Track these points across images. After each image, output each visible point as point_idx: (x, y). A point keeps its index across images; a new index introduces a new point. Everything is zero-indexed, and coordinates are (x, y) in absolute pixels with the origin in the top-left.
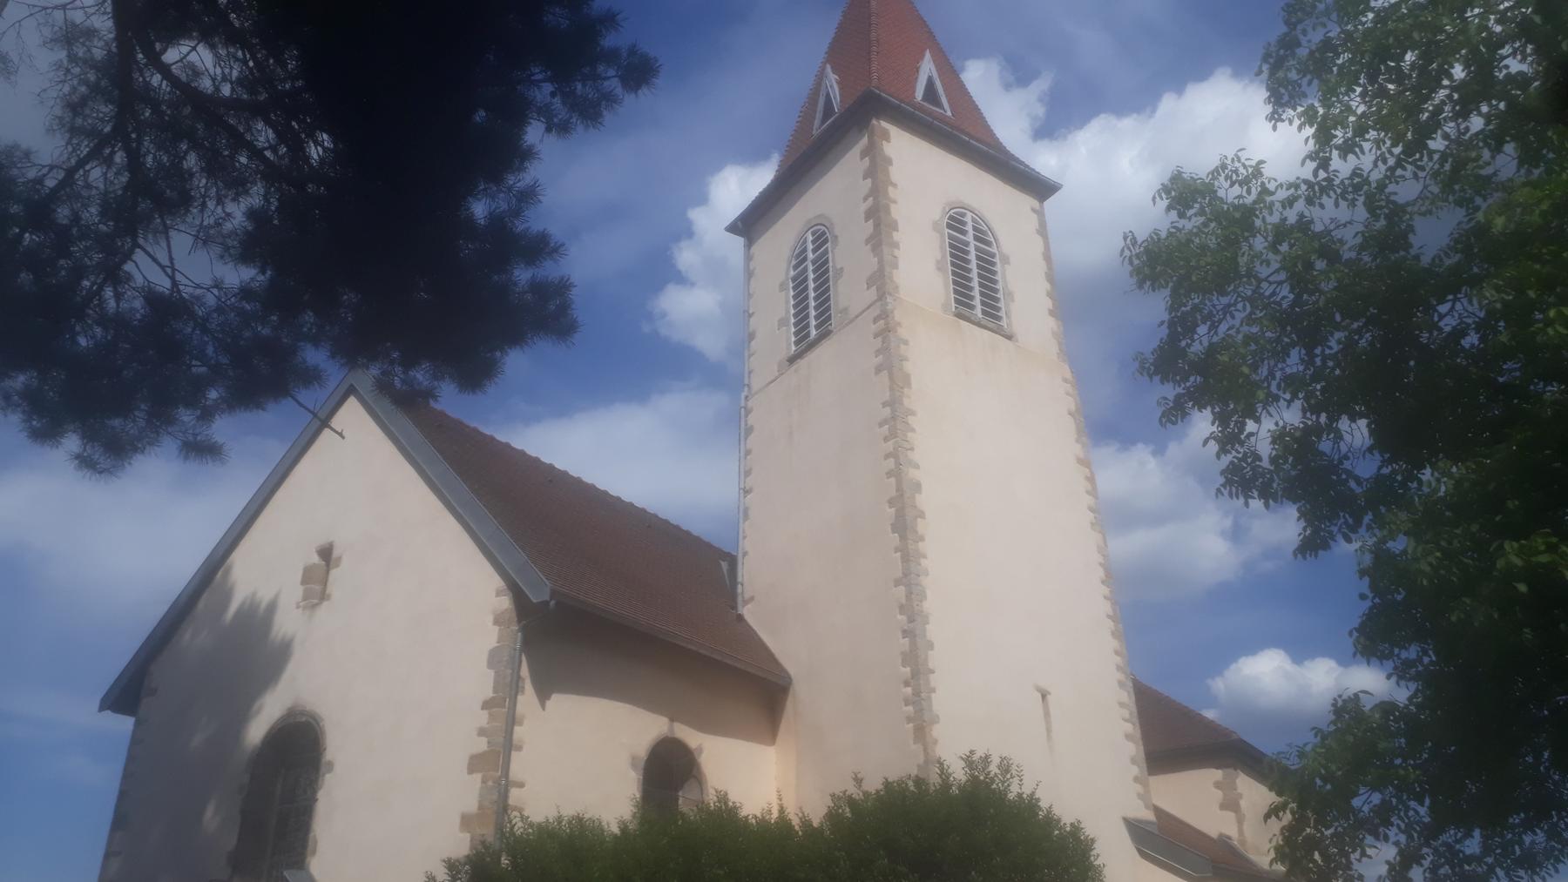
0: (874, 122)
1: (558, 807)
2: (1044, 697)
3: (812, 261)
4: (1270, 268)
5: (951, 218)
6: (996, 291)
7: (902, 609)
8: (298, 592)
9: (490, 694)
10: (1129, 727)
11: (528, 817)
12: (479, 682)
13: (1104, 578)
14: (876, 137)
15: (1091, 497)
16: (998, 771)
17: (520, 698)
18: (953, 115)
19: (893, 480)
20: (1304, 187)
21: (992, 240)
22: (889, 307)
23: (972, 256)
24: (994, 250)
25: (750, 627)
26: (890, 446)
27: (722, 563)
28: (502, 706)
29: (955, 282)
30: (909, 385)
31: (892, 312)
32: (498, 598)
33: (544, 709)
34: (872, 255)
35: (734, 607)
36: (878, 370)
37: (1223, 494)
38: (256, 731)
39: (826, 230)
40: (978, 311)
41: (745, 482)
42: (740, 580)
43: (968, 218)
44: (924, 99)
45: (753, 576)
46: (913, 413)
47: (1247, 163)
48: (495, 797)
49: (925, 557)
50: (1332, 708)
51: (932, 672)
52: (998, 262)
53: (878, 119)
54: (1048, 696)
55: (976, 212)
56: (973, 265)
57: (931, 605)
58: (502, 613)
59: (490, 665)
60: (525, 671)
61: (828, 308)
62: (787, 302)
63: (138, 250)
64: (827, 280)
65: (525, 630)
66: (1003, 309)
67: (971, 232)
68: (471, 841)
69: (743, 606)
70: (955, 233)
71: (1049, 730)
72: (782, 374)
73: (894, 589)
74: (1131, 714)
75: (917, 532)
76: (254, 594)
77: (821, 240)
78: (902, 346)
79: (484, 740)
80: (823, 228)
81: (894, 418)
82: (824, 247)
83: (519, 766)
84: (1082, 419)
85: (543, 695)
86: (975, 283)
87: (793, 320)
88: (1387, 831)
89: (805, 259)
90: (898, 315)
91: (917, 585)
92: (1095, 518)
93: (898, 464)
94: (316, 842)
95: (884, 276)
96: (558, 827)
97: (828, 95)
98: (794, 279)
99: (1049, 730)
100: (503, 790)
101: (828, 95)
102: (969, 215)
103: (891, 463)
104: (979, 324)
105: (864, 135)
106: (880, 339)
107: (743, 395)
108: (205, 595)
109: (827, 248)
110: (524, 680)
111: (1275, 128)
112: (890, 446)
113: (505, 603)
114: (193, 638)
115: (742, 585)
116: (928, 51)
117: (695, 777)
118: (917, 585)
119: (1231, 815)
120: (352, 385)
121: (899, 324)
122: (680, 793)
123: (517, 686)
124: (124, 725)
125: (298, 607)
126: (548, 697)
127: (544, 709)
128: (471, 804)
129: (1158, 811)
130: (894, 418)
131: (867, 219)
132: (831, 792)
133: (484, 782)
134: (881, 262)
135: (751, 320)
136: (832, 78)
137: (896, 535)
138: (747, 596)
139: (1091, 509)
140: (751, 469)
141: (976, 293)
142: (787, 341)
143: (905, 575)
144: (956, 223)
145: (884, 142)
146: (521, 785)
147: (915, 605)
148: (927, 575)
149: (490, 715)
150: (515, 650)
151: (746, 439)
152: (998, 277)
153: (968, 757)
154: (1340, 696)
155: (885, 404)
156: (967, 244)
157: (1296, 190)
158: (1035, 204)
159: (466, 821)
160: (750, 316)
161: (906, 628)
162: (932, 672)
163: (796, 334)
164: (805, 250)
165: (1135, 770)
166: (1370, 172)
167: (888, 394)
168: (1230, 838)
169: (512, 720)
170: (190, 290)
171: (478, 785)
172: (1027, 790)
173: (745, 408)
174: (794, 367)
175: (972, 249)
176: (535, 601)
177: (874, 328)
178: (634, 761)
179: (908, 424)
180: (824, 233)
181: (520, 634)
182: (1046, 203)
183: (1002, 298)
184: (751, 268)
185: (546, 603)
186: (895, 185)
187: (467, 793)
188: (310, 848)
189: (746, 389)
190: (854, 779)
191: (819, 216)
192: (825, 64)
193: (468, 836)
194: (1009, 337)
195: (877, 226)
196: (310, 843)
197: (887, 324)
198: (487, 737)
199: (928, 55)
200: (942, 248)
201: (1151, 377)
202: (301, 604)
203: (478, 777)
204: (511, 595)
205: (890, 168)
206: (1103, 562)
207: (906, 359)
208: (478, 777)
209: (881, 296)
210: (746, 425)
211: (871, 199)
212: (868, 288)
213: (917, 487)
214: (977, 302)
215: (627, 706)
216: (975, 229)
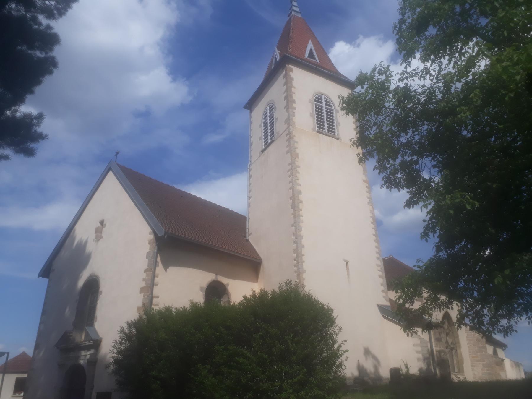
1: (338, 316)
2: (347, 263)
4: (390, 103)
9: (146, 267)
12: (143, 263)
13: (372, 221)
15: (368, 194)
18: (320, 62)
19: (291, 190)
23: (324, 111)
24: (333, 108)
26: (290, 179)
28: (151, 271)
29: (317, 120)
31: (292, 132)
33: (166, 272)
34: (286, 112)
35: (246, 237)
36: (287, 152)
38: (81, 283)
40: (326, 131)
42: (247, 227)
43: (323, 98)
44: (308, 57)
45: (251, 226)
46: (299, 167)
48: (148, 301)
49: (302, 216)
52: (334, 113)
53: (288, 64)
54: (348, 263)
55: (326, 95)
60: (159, 259)
67: (324, 103)
71: (348, 275)
74: (381, 269)
77: (271, 108)
78: (296, 144)
81: (292, 169)
83: (156, 291)
85: (166, 267)
87: (263, 137)
88: (452, 306)
89: (267, 116)
90: (294, 133)
92: (370, 201)
93: (293, 185)
95: (290, 119)
98: (264, 123)
99: (348, 275)
101: (276, 58)
102: (323, 96)
104: (326, 135)
106: (288, 142)
107: (249, 165)
112: (290, 179)
113: (152, 237)
114: (64, 254)
115: (248, 229)
117: (227, 294)
120: (110, 167)
122: (222, 299)
124: (45, 281)
125: (94, 241)
127: (166, 272)
130: (292, 169)
137: (292, 209)
139: (368, 198)
140: (251, 190)
143: (295, 223)
144: (318, 99)
145: (291, 72)
146: (158, 297)
149: (146, 274)
150: (155, 252)
152: (334, 118)
153: (286, 282)
155: (289, 164)
164: (267, 113)
165: (382, 288)
169: (154, 276)
173: (249, 169)
174: (264, 153)
176: (159, 236)
177: (286, 138)
178: (201, 289)
179: (297, 171)
181: (156, 247)
186: (294, 87)
188: (95, 320)
189: (250, 163)
194: (338, 139)
195: (288, 102)
197: (290, 136)
198: (145, 281)
199: (310, 41)
200: (312, 109)
202: (95, 240)
203: (142, 295)
205: (293, 81)
206: (372, 216)
207: (297, 148)
208: (142, 295)
211: (286, 93)
212: (285, 124)
213: (300, 192)
215: (199, 270)
216: (325, 101)
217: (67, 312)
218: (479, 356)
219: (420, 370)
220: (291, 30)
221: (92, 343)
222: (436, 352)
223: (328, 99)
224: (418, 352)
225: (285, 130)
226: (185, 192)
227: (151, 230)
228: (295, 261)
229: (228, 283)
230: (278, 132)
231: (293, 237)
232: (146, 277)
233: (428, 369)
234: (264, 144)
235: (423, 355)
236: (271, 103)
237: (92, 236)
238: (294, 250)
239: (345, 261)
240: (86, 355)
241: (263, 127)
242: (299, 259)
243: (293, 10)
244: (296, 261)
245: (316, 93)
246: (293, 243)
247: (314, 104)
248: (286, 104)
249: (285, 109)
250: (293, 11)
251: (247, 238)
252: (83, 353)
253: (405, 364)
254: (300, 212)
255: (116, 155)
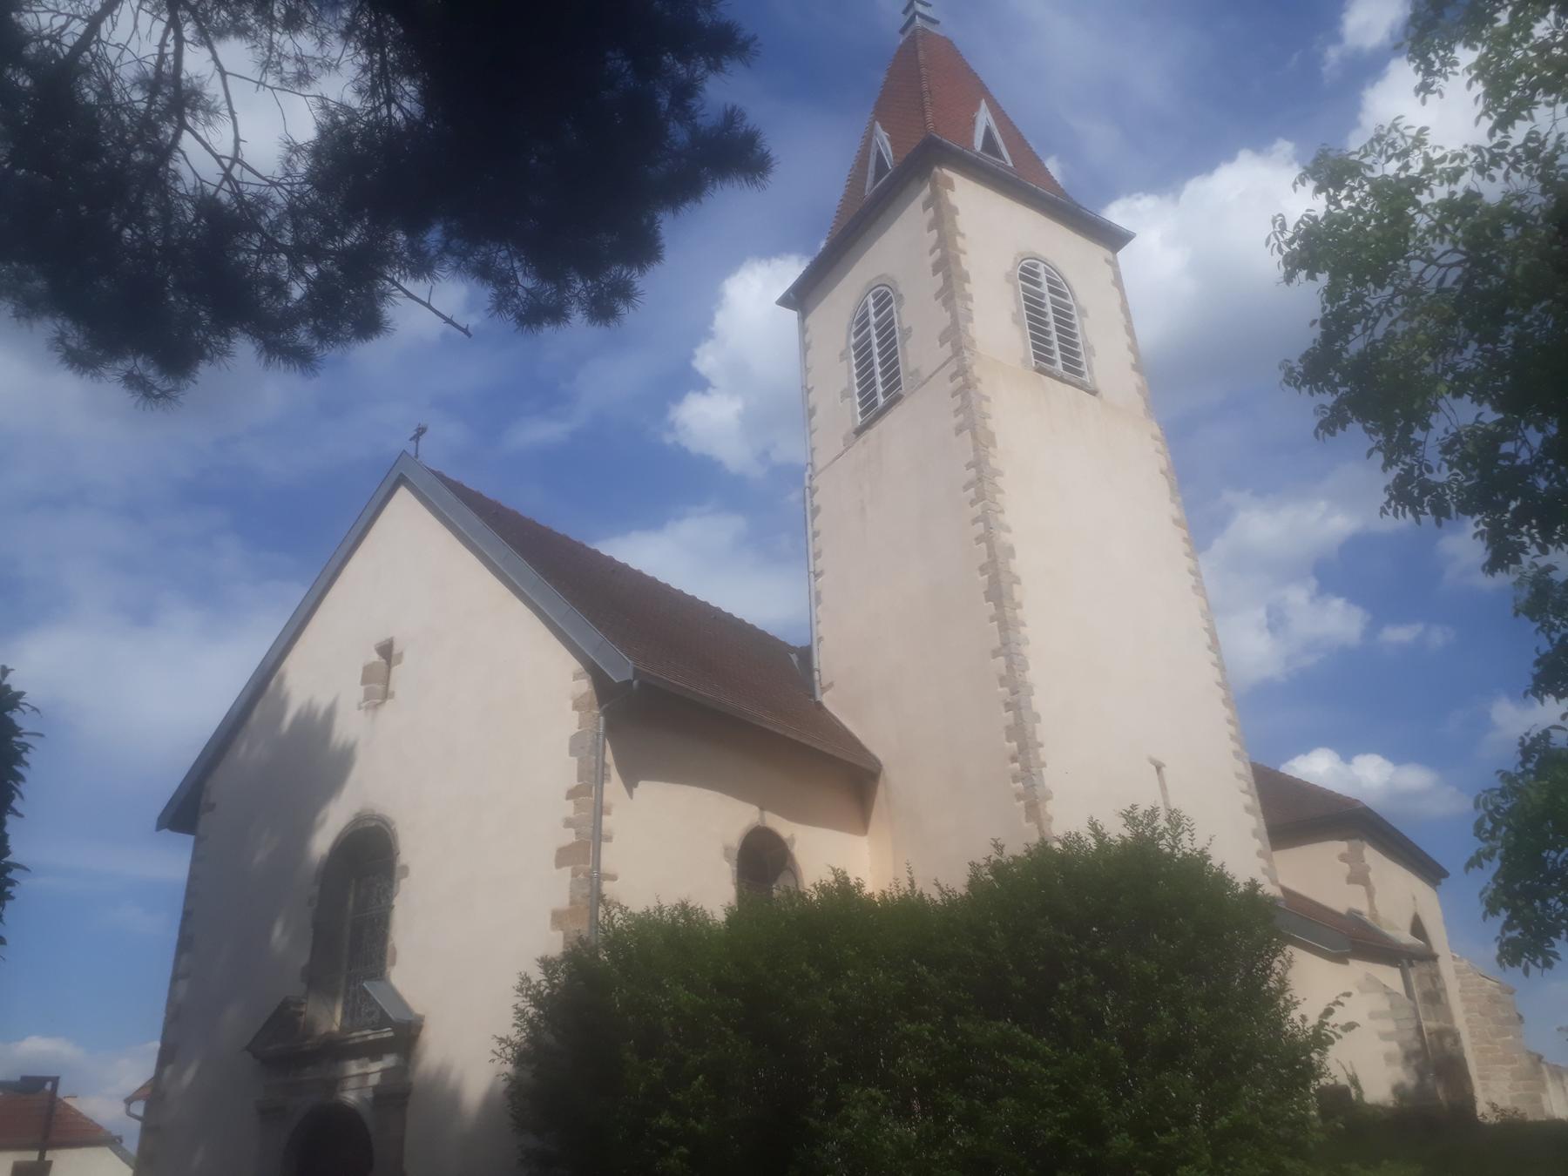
0: (936, 170)
2: (1159, 768)
3: (853, 347)
5: (1023, 269)
6: (1076, 345)
7: (1002, 681)
8: (359, 692)
9: (573, 782)
10: (1248, 799)
11: (627, 908)
12: (564, 771)
14: (938, 186)
16: (1167, 826)
17: (606, 785)
19: (983, 545)
20: (1472, 156)
21: (1068, 291)
22: (968, 362)
23: (1049, 309)
24: (1070, 301)
25: (829, 713)
27: (791, 656)
28: (588, 793)
30: (993, 443)
31: (971, 367)
32: (577, 682)
33: (631, 798)
34: (943, 309)
35: (813, 695)
36: (959, 430)
37: (1387, 513)
38: (322, 843)
39: (889, 291)
41: (814, 565)
42: (816, 666)
43: (1041, 269)
45: (827, 664)
47: (1408, 132)
48: (587, 891)
49: (1024, 625)
50: (1520, 748)
51: (1041, 745)
55: (1049, 263)
56: (1050, 318)
57: (1034, 674)
58: (581, 697)
59: (572, 752)
60: (609, 757)
61: (897, 372)
62: (850, 371)
63: (185, 132)
64: (894, 343)
65: (608, 713)
66: (1085, 363)
67: (1045, 284)
68: (565, 938)
69: (822, 694)
70: (1028, 285)
72: (849, 447)
73: (993, 660)
74: (1249, 785)
75: (1013, 599)
76: (310, 702)
79: (572, 831)
80: (885, 289)
81: (980, 480)
82: (866, 330)
83: (610, 857)
84: (1175, 478)
85: (630, 782)
86: (1054, 336)
87: (857, 390)
89: (867, 324)
90: (976, 370)
91: (1018, 654)
93: (988, 528)
94: (395, 953)
95: (959, 329)
96: (659, 918)
97: (879, 154)
98: (855, 347)
100: (595, 883)
103: (980, 528)
104: (1061, 379)
105: (926, 186)
106: (958, 397)
107: (807, 474)
108: (259, 705)
109: (892, 309)
110: (609, 766)
111: (1424, 102)
113: (585, 686)
114: (246, 751)
115: (819, 671)
116: (983, 100)
118: (1018, 654)
119: (1361, 889)
120: (401, 475)
121: (979, 380)
123: (603, 774)
125: (360, 708)
126: (636, 785)
127: (631, 798)
128: (562, 900)
129: (1284, 890)
130: (980, 480)
131: (935, 272)
132: (970, 861)
133: (574, 875)
134: (954, 317)
135: (810, 396)
136: (882, 137)
137: (992, 603)
138: (825, 683)
139: (1192, 572)
141: (1056, 346)
142: (852, 411)
143: (1004, 645)
144: (1028, 274)
145: (948, 190)
146: (613, 878)
147: (1017, 676)
148: (1028, 643)
151: (812, 521)
152: (1077, 330)
153: (1129, 812)
154: (1527, 734)
155: (969, 466)
156: (1042, 296)
157: (1462, 162)
158: (1107, 253)
159: (558, 918)
160: (809, 391)
161: (1008, 700)
162: (1041, 745)
163: (861, 404)
164: (866, 314)
165: (1257, 844)
166: (1548, 134)
167: (972, 454)
168: (1360, 913)
169: (600, 810)
170: (254, 189)
171: (568, 878)
172: (1198, 845)
173: (809, 488)
175: (1047, 301)
176: (617, 681)
177: (951, 386)
180: (887, 294)
181: (602, 718)
182: (1119, 254)
183: (1083, 353)
184: (807, 341)
185: (629, 683)
186: (963, 236)
187: (558, 888)
190: (994, 846)
191: (880, 277)
192: (874, 121)
193: (560, 934)
194: (1094, 393)
196: (389, 954)
197: (966, 380)
198: (574, 828)
201: (1299, 388)
202: (363, 705)
203: (567, 870)
204: (590, 678)
205: (957, 217)
208: (567, 870)
209: (958, 351)
210: (812, 505)
213: (1011, 552)
214: (1057, 356)
216: (1049, 280)
217: (278, 934)
218: (1499, 1047)
219: (1398, 1090)
220: (923, 70)
221: (391, 1034)
222: (1430, 1034)
223: (1057, 275)
224: (1385, 1036)
225: (945, 364)
226: (611, 560)
227: (581, 667)
228: (1013, 762)
229: (792, 835)
230: (917, 371)
231: (1000, 690)
232: (575, 814)
233: (1420, 1086)
234: (859, 410)
235: (1401, 1045)
236: (879, 286)
237: (351, 691)
238: (1008, 728)
239: (1154, 764)
240: (366, 1075)
241: (853, 359)
242: (1031, 756)
243: (917, 13)
244: (1016, 761)
245: (1022, 255)
246: (1002, 708)
247: (1020, 288)
248: (942, 284)
249: (940, 300)
250: (917, 17)
251: (818, 700)
252: (353, 1067)
253: (1348, 1075)
254: (1017, 611)
255: (416, 438)
